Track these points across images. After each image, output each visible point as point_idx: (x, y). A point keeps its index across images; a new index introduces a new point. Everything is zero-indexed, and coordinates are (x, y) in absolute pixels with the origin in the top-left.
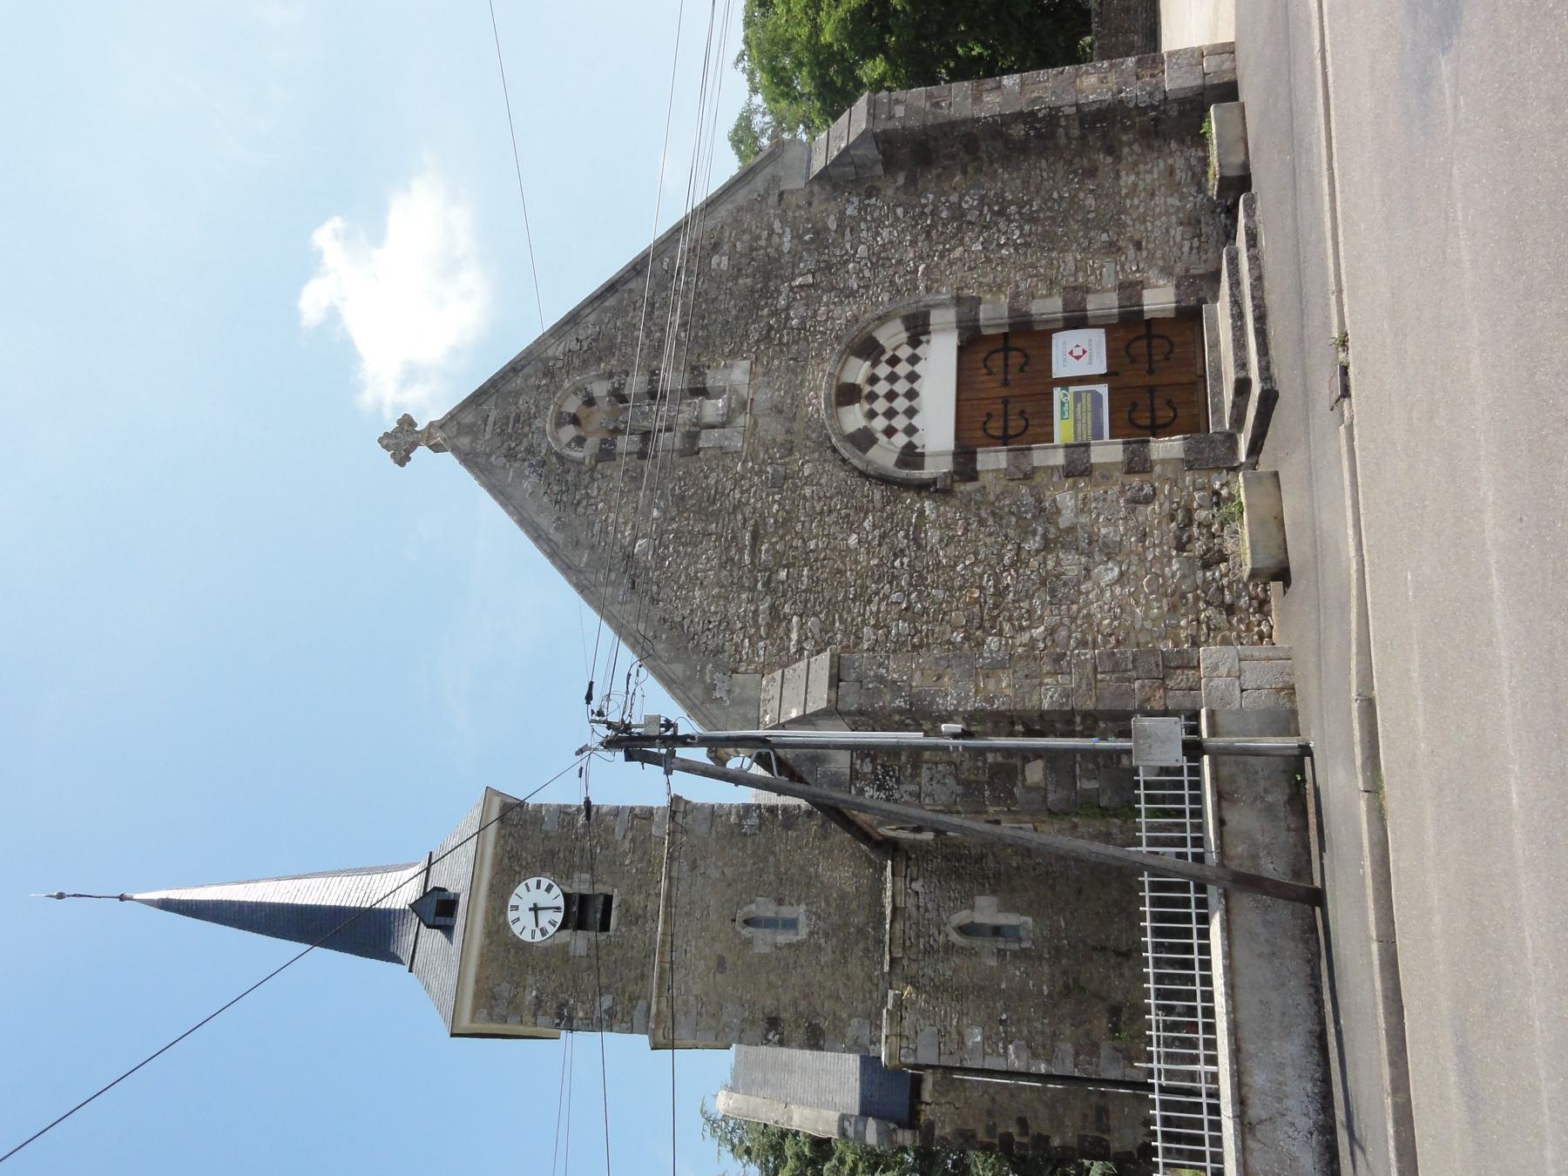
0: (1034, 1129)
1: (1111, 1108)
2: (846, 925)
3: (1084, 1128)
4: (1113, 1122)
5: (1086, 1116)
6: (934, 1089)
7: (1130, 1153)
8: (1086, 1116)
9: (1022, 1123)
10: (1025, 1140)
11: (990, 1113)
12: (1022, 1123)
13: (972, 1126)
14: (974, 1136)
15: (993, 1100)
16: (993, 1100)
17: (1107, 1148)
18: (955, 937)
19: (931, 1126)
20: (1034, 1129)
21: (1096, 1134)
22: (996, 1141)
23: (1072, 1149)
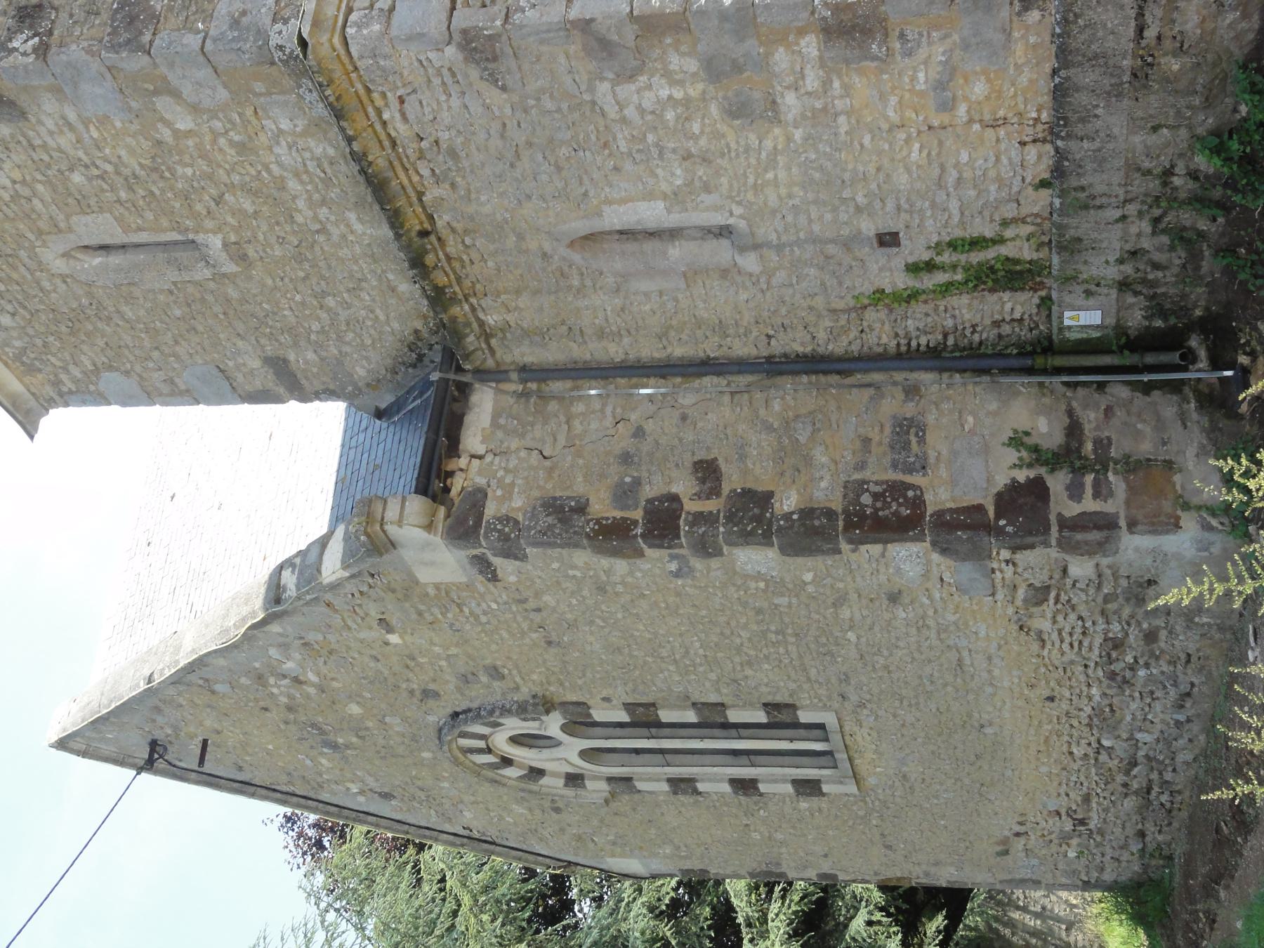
0: (732, 481)
1: (931, 418)
2: (630, 154)
3: (861, 466)
4: (937, 444)
5: (866, 441)
6: (495, 424)
7: (980, 508)
8: (866, 441)
9: (708, 472)
10: (711, 505)
11: (626, 458)
12: (708, 472)
13: (579, 487)
14: (581, 509)
15: (639, 433)
16: (639, 433)
17: (918, 503)
18: (604, 911)
19: (477, 498)
20: (732, 481)
21: (893, 476)
22: (638, 515)
23: (830, 514)
